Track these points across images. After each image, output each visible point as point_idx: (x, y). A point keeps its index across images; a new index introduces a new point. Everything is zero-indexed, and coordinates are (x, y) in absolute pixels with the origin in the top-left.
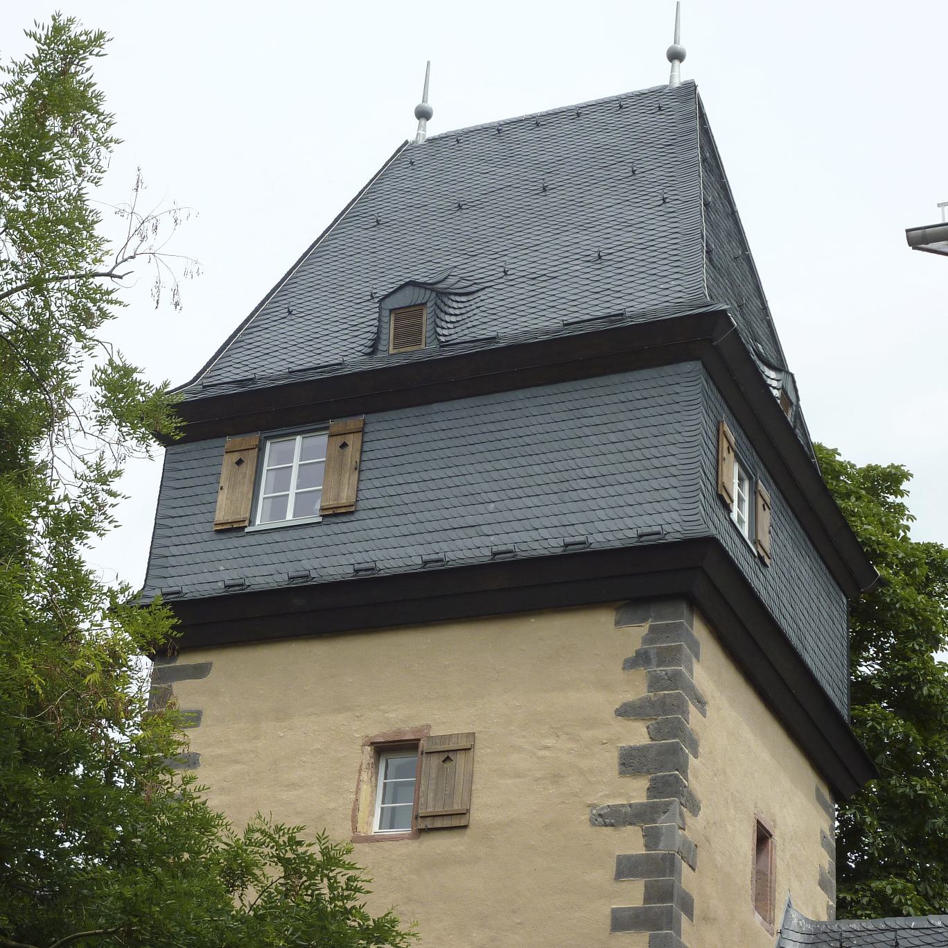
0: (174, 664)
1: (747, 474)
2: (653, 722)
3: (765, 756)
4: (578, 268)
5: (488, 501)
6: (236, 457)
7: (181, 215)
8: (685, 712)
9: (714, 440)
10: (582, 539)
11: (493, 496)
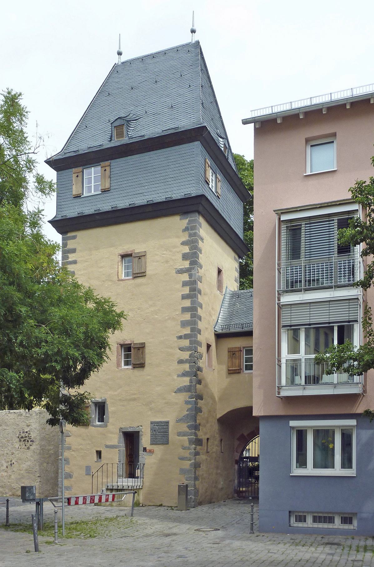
1: (214, 172)
3: (220, 250)
4: (166, 110)
6: (76, 175)
7: (50, 135)
8: (198, 243)
10: (170, 196)
11: (147, 184)
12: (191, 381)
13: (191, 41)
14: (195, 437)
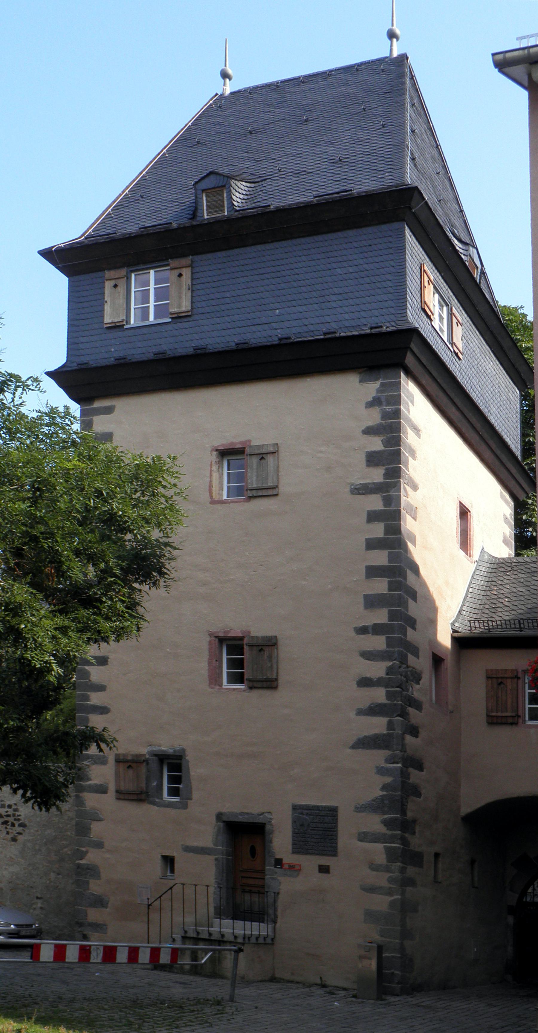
0: (92, 407)
2: (385, 437)
5: (275, 308)
6: (113, 283)
9: (419, 277)
12: (390, 725)
13: (388, 55)
14: (402, 847)
